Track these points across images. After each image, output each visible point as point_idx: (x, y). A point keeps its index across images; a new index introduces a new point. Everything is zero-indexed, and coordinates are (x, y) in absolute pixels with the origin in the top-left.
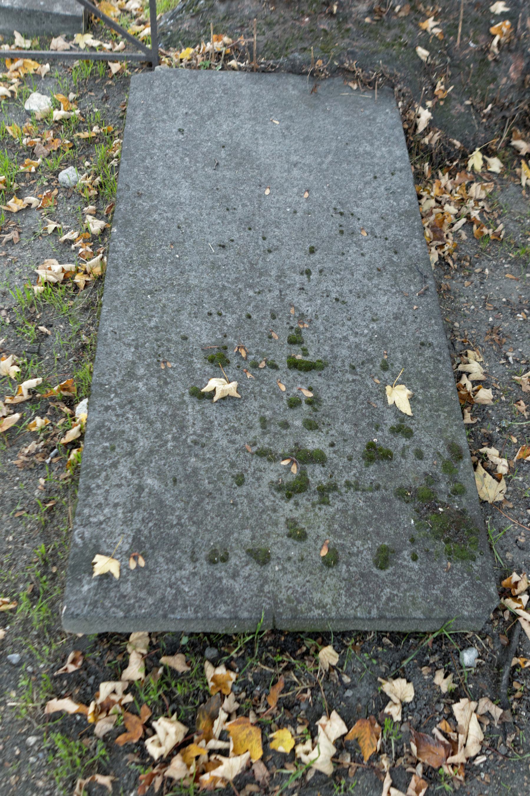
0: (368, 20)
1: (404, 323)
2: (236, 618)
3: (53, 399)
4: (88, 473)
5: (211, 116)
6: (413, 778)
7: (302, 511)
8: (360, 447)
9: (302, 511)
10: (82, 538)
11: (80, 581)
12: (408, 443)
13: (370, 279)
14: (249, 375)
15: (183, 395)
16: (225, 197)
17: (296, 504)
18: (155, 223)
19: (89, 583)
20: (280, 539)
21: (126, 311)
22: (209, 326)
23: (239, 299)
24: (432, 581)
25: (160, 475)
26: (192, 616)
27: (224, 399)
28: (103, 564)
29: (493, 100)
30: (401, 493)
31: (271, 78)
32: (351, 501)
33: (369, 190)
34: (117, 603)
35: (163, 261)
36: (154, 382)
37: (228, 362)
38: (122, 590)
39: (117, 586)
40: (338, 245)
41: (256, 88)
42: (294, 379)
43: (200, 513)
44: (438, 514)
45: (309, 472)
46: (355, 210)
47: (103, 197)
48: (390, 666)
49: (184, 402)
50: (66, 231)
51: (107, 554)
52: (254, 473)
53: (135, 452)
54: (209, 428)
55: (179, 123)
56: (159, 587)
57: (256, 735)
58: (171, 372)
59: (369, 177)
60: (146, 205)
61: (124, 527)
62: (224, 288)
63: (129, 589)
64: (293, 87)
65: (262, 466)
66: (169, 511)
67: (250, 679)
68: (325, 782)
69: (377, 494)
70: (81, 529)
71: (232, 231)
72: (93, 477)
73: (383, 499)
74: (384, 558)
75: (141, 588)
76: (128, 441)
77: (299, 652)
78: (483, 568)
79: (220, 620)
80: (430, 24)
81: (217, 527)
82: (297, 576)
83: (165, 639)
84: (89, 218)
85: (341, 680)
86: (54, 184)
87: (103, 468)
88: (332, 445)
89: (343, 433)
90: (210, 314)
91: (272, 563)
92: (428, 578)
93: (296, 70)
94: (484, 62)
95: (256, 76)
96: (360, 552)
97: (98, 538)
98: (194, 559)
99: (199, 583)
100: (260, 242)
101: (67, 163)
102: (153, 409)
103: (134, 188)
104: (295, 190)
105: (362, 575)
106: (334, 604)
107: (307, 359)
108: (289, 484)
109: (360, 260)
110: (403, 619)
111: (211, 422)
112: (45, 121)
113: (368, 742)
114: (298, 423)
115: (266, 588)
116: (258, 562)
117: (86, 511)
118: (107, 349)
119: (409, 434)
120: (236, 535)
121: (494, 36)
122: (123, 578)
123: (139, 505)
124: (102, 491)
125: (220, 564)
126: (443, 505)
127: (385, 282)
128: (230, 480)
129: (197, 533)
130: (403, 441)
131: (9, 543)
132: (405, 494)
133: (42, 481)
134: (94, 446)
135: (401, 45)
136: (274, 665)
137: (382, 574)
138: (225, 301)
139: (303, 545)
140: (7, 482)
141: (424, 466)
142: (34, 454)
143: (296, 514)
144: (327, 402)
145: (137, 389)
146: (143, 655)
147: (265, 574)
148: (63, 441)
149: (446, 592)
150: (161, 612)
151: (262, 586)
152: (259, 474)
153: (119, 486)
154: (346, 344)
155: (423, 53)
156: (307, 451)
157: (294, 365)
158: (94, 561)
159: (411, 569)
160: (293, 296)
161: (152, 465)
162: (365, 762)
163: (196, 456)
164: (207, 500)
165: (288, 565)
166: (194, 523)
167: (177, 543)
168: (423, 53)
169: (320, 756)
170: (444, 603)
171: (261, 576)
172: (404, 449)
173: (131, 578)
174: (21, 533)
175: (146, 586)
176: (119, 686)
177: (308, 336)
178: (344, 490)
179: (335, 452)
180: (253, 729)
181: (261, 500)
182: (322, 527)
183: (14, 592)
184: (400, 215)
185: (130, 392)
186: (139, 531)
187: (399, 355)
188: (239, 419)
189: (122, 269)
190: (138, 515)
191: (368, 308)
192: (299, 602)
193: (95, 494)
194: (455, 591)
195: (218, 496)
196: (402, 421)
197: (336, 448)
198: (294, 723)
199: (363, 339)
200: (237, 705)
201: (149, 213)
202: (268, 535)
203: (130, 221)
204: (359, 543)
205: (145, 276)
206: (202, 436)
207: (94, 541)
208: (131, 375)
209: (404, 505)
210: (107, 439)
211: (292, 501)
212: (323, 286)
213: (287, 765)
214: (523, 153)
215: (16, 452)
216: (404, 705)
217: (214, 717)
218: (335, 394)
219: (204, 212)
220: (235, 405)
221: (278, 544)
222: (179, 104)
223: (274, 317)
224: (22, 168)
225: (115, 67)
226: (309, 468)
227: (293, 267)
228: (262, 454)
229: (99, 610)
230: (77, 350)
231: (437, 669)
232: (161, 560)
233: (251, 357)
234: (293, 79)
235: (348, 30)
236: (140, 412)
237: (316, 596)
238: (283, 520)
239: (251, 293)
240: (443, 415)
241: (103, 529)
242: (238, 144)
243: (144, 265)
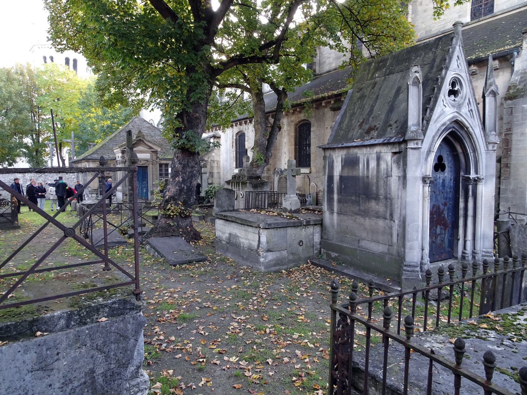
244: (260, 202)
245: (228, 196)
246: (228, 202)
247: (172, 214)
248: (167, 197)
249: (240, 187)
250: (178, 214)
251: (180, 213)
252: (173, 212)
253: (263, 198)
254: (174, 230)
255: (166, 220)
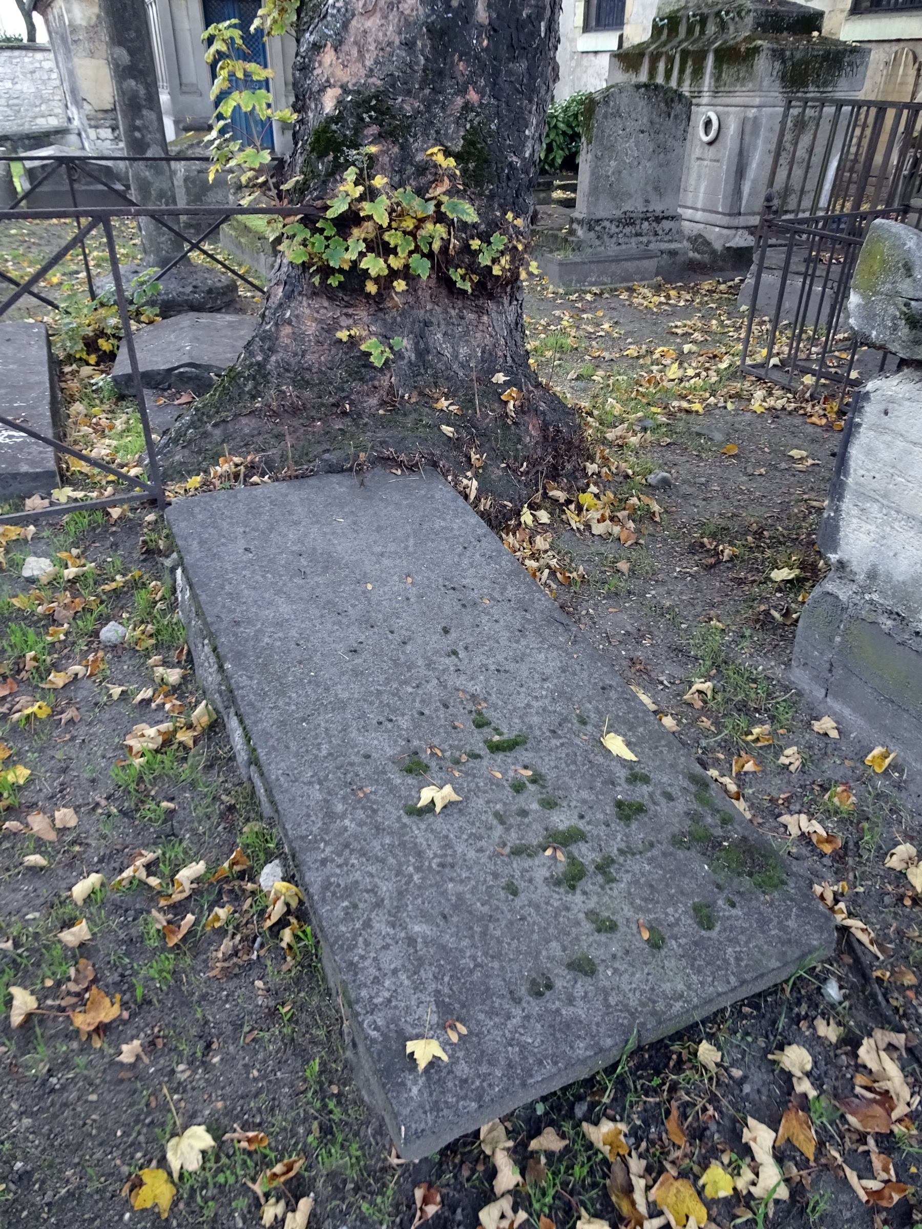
0: (381, 412)
1: (574, 674)
2: (601, 1050)
3: (226, 880)
4: (342, 946)
5: (271, 529)
6: (873, 1157)
7: (595, 899)
8: (610, 809)
9: (595, 899)
10: (377, 1029)
11: (403, 1084)
12: (650, 789)
13: (517, 642)
14: (457, 774)
15: (399, 818)
16: (329, 602)
17: (585, 893)
18: (270, 647)
19: (415, 1082)
20: (591, 939)
21: (287, 747)
22: (386, 735)
23: (400, 699)
24: (763, 923)
25: (425, 916)
26: (554, 1070)
27: (445, 807)
28: (424, 1051)
29: (526, 458)
30: (676, 841)
31: (312, 481)
32: (636, 868)
33: (466, 561)
34: (462, 1093)
35: (299, 683)
36: (360, 814)
37: (427, 766)
38: (458, 1074)
39: (451, 1072)
40: (468, 619)
41: (303, 494)
42: (504, 762)
43: (493, 943)
44: (725, 848)
45: (576, 854)
46: (464, 582)
47: (165, 643)
48: (767, 1037)
49: (405, 826)
50: (139, 690)
51: (418, 1037)
52: (522, 876)
53: (383, 900)
54: (447, 845)
55: (241, 544)
56: (498, 1051)
57: (684, 1188)
58: (373, 797)
59: (460, 549)
60: (251, 631)
61: (419, 995)
62: (379, 693)
63: (466, 1069)
64: (339, 485)
65: (526, 865)
66: (458, 954)
67: (638, 1123)
68: (789, 1212)
69: (655, 852)
70: (370, 1018)
71: (356, 634)
72: (351, 948)
73: (665, 854)
74: (705, 917)
75: (478, 1062)
76: (368, 891)
77: (672, 1064)
78: (798, 888)
79: (583, 1062)
80: (443, 403)
81: (520, 952)
82: (633, 974)
83: (518, 1117)
84: (160, 670)
85: (731, 1077)
86: (95, 645)
87: (356, 934)
88: (582, 817)
89: (584, 802)
90: (380, 723)
91: (601, 969)
92: (758, 921)
93: (334, 469)
94: (506, 427)
95: (297, 483)
96: (678, 920)
97: (394, 1020)
98: (518, 1001)
99: (539, 1026)
100: (390, 636)
101: (104, 620)
102: (376, 844)
103: (227, 618)
104: (396, 578)
105: (696, 944)
106: (689, 988)
107: (505, 737)
108: (564, 873)
109: (497, 627)
110: (762, 976)
111: (447, 837)
112: (54, 583)
113: (802, 1137)
114: (535, 806)
115: (612, 1001)
116: (586, 974)
117: (364, 993)
118: (288, 796)
119: (646, 780)
120: (544, 953)
121: (506, 403)
122: (454, 1060)
123: (421, 961)
124: (369, 961)
125: (548, 993)
126: (726, 839)
127: (532, 640)
128: (502, 894)
129: (502, 968)
130: (645, 789)
131: (255, 1080)
132: (682, 842)
133: (259, 984)
134: (331, 911)
135: (425, 426)
136: (656, 1091)
137: (714, 934)
138: (388, 705)
139: (618, 935)
140: (213, 1003)
141: (680, 806)
142: (231, 956)
143: (591, 904)
144: (551, 776)
145: (346, 829)
146: (508, 1149)
147: (601, 984)
148: (269, 923)
149: (783, 928)
150: (517, 1082)
151: (606, 999)
152: (527, 875)
153: (386, 947)
154: (533, 711)
155: (448, 430)
156: (563, 833)
157: (495, 748)
158: (408, 1051)
159: (737, 918)
160: (453, 680)
161: (410, 908)
162: (812, 1164)
163: (451, 880)
164: (491, 926)
165: (617, 965)
166: (492, 957)
167: (488, 989)
168: (448, 430)
169: (770, 1180)
170: (789, 941)
171: (597, 988)
172: (651, 795)
173: (460, 1054)
174: (264, 1061)
175: (482, 1057)
176: (505, 1204)
177: (490, 714)
178: (621, 860)
179: (588, 823)
180: (679, 1184)
181: (547, 903)
182: (626, 909)
183: (296, 1144)
184: (509, 575)
185: (340, 834)
186: (437, 992)
187: (589, 706)
188: (473, 824)
189: (259, 705)
190: (427, 973)
191: (532, 670)
192: (654, 1002)
193: (364, 968)
194: (792, 923)
195: (500, 916)
196: (632, 769)
197: (587, 819)
198: (714, 1153)
199: (547, 701)
200: (644, 1163)
201: (256, 638)
202: (577, 939)
203: (239, 652)
204: (670, 910)
205: (289, 704)
206: (446, 855)
207: (392, 1026)
208: (330, 816)
209: (687, 853)
210: (342, 898)
211: (578, 892)
212: (477, 661)
213: (738, 1211)
214: (562, 501)
215: (205, 961)
216: (808, 1074)
217: (629, 1189)
218: (552, 764)
219: (316, 622)
220: (460, 810)
221: (594, 946)
222: (232, 525)
223: (446, 706)
224: (49, 639)
225: (115, 512)
226: (574, 848)
227: (436, 652)
228: (517, 852)
229: (446, 1112)
230: (222, 816)
231: (814, 1018)
232: (481, 1016)
233: (448, 754)
234: (335, 478)
235: (366, 424)
236: (363, 853)
237: (667, 987)
238: (582, 916)
239: (410, 690)
240: (665, 750)
241: (396, 1007)
242: (314, 549)
243: (282, 693)
244: (798, 172)
245: (653, 130)
246: (649, 167)
247: (374, 265)
248: (329, 103)
249: (708, 81)
250: (423, 268)
251: (441, 262)
252: (387, 250)
253: (819, 150)
254: (391, 402)
255: (327, 310)
